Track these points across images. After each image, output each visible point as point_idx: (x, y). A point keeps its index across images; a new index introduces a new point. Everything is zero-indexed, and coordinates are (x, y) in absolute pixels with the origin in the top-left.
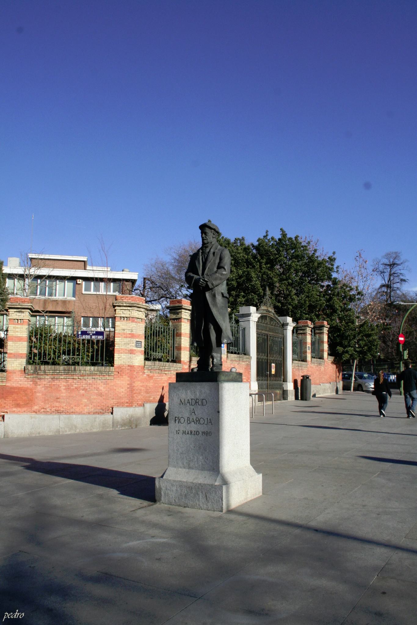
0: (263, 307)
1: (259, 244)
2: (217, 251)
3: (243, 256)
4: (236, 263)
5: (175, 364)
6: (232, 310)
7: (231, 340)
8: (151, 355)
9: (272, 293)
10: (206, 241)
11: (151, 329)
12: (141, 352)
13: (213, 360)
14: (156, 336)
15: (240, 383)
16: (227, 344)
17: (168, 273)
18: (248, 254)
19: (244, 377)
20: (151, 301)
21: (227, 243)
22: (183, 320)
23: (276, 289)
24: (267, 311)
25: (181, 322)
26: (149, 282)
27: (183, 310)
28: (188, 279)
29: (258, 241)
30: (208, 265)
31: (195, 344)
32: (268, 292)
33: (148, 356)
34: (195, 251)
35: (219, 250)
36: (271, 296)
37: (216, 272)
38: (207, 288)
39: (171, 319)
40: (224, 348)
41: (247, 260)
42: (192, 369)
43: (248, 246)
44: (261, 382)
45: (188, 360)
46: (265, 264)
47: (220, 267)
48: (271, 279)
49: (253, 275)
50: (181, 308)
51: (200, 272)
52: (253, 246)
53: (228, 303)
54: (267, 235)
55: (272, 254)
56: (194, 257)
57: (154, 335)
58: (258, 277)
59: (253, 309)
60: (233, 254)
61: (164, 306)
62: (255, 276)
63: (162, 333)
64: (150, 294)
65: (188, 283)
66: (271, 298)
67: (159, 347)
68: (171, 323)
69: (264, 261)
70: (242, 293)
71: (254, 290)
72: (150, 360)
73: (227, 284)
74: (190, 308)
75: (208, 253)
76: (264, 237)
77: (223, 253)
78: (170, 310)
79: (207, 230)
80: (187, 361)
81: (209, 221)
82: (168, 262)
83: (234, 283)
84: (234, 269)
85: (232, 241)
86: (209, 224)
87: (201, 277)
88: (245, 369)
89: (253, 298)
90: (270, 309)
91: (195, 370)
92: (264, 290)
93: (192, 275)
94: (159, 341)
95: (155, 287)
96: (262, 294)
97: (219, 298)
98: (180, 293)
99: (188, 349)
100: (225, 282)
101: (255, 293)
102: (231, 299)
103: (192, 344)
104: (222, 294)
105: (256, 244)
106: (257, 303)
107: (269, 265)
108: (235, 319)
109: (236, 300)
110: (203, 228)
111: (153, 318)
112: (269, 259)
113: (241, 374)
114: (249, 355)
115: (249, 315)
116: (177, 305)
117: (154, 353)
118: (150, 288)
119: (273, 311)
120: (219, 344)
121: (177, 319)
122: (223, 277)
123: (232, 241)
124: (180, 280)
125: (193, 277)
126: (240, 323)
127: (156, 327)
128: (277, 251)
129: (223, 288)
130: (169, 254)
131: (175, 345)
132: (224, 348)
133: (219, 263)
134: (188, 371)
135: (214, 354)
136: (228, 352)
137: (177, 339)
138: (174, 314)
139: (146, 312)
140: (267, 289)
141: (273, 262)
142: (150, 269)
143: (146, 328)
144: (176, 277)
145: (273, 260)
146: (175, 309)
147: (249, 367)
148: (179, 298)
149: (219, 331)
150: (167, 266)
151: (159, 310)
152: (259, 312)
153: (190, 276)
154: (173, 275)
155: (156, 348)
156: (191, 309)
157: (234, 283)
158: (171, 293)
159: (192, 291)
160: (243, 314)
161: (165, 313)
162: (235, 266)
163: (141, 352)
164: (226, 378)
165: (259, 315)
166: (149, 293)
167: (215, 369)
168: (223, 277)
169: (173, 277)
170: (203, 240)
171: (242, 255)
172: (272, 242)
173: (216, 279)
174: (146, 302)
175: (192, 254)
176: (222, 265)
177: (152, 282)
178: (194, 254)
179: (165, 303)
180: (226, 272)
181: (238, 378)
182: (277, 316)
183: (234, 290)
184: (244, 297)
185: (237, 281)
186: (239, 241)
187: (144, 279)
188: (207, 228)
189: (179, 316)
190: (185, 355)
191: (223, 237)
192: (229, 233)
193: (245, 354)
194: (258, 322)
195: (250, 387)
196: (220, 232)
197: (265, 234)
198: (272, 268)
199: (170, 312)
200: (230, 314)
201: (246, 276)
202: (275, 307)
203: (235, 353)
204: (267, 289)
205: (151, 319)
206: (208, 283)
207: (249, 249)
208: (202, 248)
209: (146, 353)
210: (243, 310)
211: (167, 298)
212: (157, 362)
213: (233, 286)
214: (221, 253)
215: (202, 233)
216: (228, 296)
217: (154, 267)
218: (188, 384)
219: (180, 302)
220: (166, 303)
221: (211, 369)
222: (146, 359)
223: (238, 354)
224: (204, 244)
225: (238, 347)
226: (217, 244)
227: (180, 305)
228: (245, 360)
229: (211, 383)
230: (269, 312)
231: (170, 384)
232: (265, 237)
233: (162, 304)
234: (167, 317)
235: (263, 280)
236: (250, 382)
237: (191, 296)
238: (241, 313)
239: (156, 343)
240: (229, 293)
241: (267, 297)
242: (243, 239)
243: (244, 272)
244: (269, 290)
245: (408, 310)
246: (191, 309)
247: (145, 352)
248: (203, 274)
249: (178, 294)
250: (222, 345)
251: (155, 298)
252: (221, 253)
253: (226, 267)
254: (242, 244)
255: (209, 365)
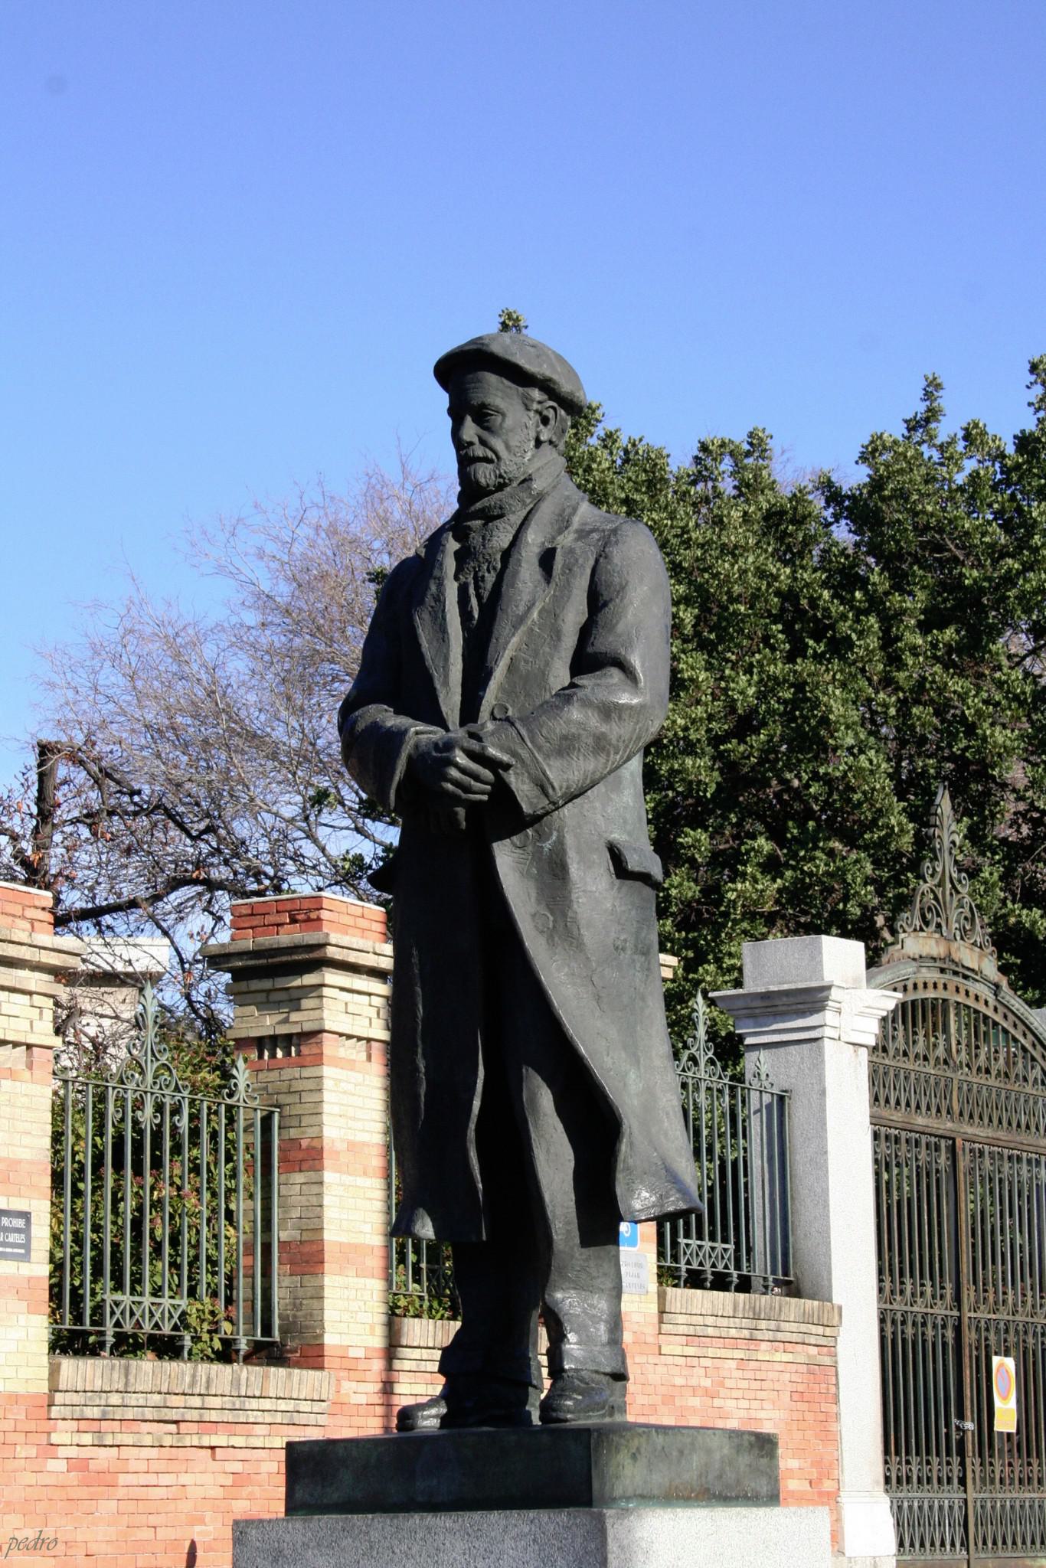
0: (916, 943)
1: (877, 484)
2: (566, 540)
3: (761, 573)
4: (709, 622)
5: (277, 1373)
6: (690, 966)
7: (684, 1192)
8: (98, 1309)
9: (975, 836)
10: (484, 474)
11: (100, 1117)
12: (20, 1289)
13: (557, 1337)
14: (138, 1171)
15: (762, 1512)
16: (660, 1220)
17: (216, 704)
18: (791, 556)
19: (787, 1461)
20: (93, 914)
21: (637, 484)
22: (330, 1046)
23: (1010, 806)
24: (949, 966)
25: (318, 1060)
26: (80, 776)
27: (331, 977)
28: (365, 751)
29: (863, 458)
30: (509, 648)
31: (426, 1229)
32: (950, 828)
33: (78, 1318)
34: (412, 546)
35: (583, 534)
36: (969, 855)
37: (567, 695)
38: (503, 815)
39: (242, 1043)
40: (638, 1250)
41: (789, 596)
42: (406, 1416)
43: (798, 498)
44: (915, 1495)
45: (377, 1340)
46: (924, 627)
47: (588, 660)
48: (971, 730)
49: (837, 705)
50: (314, 959)
51: (451, 701)
52: (834, 496)
53: (662, 913)
54: (932, 415)
55: (968, 550)
56: (404, 589)
57: (118, 1166)
58: (872, 721)
59: (840, 957)
60: (687, 557)
61: (190, 949)
62: (854, 716)
63: (177, 1149)
64: (87, 864)
65: (361, 778)
66: (973, 873)
67: (157, 1249)
68: (242, 1075)
69: (916, 602)
70: (754, 838)
71: (846, 821)
72: (94, 1351)
73: (650, 779)
74: (383, 955)
75: (506, 555)
76: (912, 425)
77: (617, 554)
78: (238, 975)
79: (495, 390)
80: (370, 1348)
81: (510, 324)
82: (219, 627)
83: (702, 770)
84: (695, 666)
85: (680, 460)
86: (504, 347)
87: (458, 733)
88: (799, 1396)
89: (839, 875)
90: (968, 956)
91: (429, 1421)
92: (922, 815)
93: (392, 720)
94: (158, 1204)
95: (123, 806)
96: (906, 843)
97: (592, 887)
98: (308, 849)
99: (376, 1262)
100: (635, 766)
101: (851, 840)
102: (684, 887)
103: (399, 1228)
104: (616, 856)
105: (853, 477)
106: (868, 914)
107: (949, 634)
108: (712, 1035)
109: (713, 893)
110: (463, 372)
111: (116, 1037)
112: (954, 585)
113: (765, 1444)
114: (821, 1292)
115: (811, 1000)
116: (287, 937)
117: (126, 1298)
118: (90, 818)
119: (990, 967)
120: (600, 1221)
121: (287, 1041)
122: (615, 731)
123: (680, 460)
124: (307, 756)
125: (399, 735)
126: (749, 1061)
127: (139, 1105)
128: (1008, 527)
129: (619, 812)
130: (220, 569)
131: (279, 1234)
132: (638, 1250)
133: (586, 632)
134: (371, 1426)
135: (566, 1299)
136: (667, 1275)
137: (289, 1186)
138: (268, 1002)
139: (63, 993)
140: (944, 803)
141: (982, 610)
142: (82, 680)
143: (59, 1112)
144: (279, 733)
145: (978, 591)
146: (274, 970)
147: (820, 1386)
148: (301, 886)
149: (596, 1126)
150: (209, 651)
151: (154, 978)
152: (885, 975)
153: (375, 727)
154: (258, 721)
155: (137, 1259)
156: (387, 964)
157: (702, 770)
158: (239, 847)
159: (392, 835)
160: (767, 996)
161: (198, 996)
162: (704, 646)
163: (20, 1289)
164: (659, 1479)
165: (889, 1001)
166: (83, 858)
167: (575, 1414)
168: (615, 731)
169: (253, 737)
170: (466, 461)
171: (750, 566)
172: (970, 465)
173: (566, 746)
174: (61, 921)
175: (387, 563)
176: (602, 643)
177: (102, 776)
178: (405, 567)
179: (199, 921)
180: (640, 697)
181: (743, 1471)
182: (1017, 1004)
183: (697, 821)
184: (772, 867)
185: (719, 756)
186: (727, 465)
187: (45, 750)
188: (492, 379)
189: (300, 1020)
190: (352, 1304)
191: (609, 439)
192: (657, 403)
193: (793, 1289)
194: (880, 1049)
195: (836, 1537)
196: (590, 395)
197: (921, 408)
198: (971, 655)
199: (237, 995)
200: (675, 999)
201: (788, 717)
202: (1007, 940)
203: (721, 1283)
204: (944, 803)
205: (99, 1048)
206: (512, 778)
207: (800, 521)
208: (457, 525)
209: (62, 1295)
210: (770, 962)
211: (211, 885)
212: (147, 1367)
213: (693, 787)
214: (602, 556)
215: (457, 413)
216: (657, 872)
217: (116, 659)
218: (377, 1526)
219: (306, 913)
220: (202, 926)
221: (546, 1407)
222: (69, 1342)
223: (744, 1286)
224: (470, 491)
225: (736, 1240)
226: (569, 488)
227: (311, 938)
228: (791, 1330)
229: (544, 1516)
230: (967, 974)
231: (242, 1530)
232: (921, 424)
233: (180, 933)
234: (212, 1024)
235: (908, 739)
236: (831, 1499)
237: (388, 878)
238: (751, 986)
239: (137, 1224)
240: (665, 846)
241: (946, 865)
242: (757, 444)
243: (768, 687)
244: (960, 812)
245: (171, 1154)
246: (387, 964)
247: (55, 1294)
248: (470, 711)
249: (297, 857)
250: (624, 1227)
251: (127, 891)
252: (602, 556)
253: (636, 661)
254: (748, 488)
255: (524, 1382)
